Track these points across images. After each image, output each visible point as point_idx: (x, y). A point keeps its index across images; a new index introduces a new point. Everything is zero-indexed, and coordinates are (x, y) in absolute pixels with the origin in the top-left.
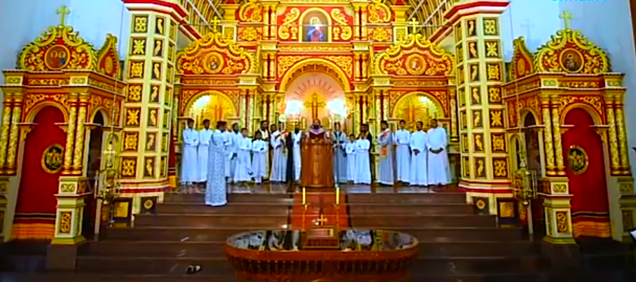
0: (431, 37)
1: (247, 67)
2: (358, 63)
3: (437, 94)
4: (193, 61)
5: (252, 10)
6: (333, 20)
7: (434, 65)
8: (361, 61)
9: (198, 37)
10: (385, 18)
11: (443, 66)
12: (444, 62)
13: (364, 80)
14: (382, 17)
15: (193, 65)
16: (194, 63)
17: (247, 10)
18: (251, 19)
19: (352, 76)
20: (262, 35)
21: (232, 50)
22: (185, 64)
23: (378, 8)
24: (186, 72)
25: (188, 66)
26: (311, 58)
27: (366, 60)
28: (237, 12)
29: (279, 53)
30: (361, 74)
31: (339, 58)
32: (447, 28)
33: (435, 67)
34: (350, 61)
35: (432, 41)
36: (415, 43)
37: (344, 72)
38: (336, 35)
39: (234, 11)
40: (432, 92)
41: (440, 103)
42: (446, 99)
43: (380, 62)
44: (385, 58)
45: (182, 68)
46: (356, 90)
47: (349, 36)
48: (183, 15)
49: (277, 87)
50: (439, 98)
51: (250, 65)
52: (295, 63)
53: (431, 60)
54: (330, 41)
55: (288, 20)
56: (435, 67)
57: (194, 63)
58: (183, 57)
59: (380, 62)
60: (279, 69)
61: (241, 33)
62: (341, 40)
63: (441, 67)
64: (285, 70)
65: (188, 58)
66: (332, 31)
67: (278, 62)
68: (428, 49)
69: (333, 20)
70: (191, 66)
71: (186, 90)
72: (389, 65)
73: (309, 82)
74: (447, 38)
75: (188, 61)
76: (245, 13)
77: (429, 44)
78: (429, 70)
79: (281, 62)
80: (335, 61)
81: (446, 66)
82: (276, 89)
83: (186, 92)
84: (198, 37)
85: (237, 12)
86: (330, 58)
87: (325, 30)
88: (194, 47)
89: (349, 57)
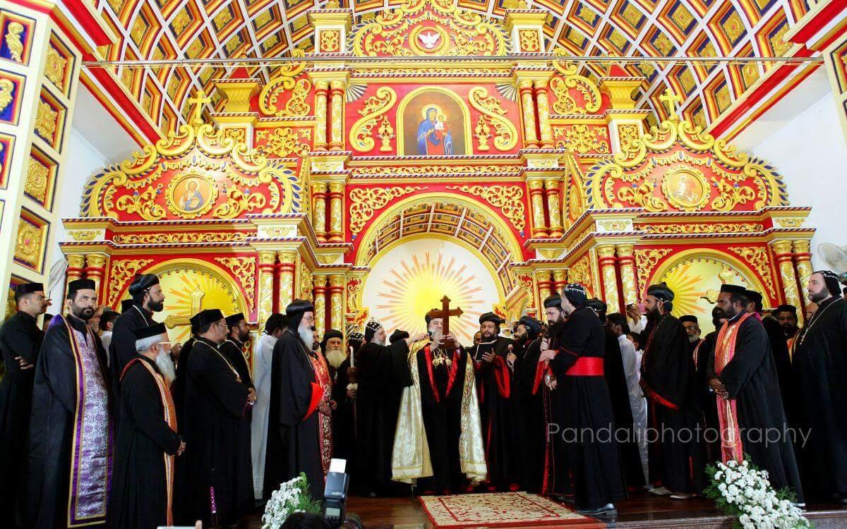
0: (711, 127)
1: (275, 200)
2: (537, 200)
3: (746, 252)
4: (141, 190)
5: (288, 93)
6: (472, 108)
7: (729, 188)
8: (544, 194)
9: (154, 138)
10: (589, 106)
11: (749, 190)
12: (749, 181)
13: (554, 235)
14: (582, 103)
15: (143, 200)
16: (145, 196)
17: (277, 92)
18: (287, 111)
19: (527, 229)
20: (311, 143)
21: (239, 163)
22: (123, 199)
23: (572, 84)
24: (123, 215)
25: (129, 202)
26: (426, 191)
27: (558, 191)
28: (254, 100)
29: (352, 182)
30: (547, 222)
31: (492, 189)
32: (793, 68)
33: (731, 192)
34: (518, 197)
35: (716, 133)
36: (678, 139)
37: (507, 220)
38: (483, 140)
39: (246, 95)
40: (736, 250)
41: (756, 272)
42: (769, 265)
43: (603, 183)
44: (613, 174)
45: (114, 209)
46: (540, 257)
47: (512, 144)
48: (101, 38)
49: (351, 257)
50: (751, 261)
51: (282, 196)
52: (391, 203)
53: (719, 177)
54: (469, 151)
55: (370, 111)
56: (731, 192)
57: (145, 196)
58: (117, 182)
59: (603, 183)
60: (354, 217)
61: (263, 142)
62: (494, 150)
63: (744, 192)
64: (366, 218)
65: (129, 185)
66: (474, 132)
67: (349, 202)
68: (709, 153)
69: (472, 108)
70: (137, 203)
71: (120, 258)
72: (624, 190)
73: (415, 259)
74: (754, 123)
75: (131, 192)
76: (273, 99)
77: (710, 142)
78: (718, 199)
79: (357, 202)
80: (485, 195)
81: (757, 191)
82: (346, 260)
83: (121, 264)
84: (154, 138)
85: (254, 100)
86: (472, 190)
87: (455, 125)
88: (147, 159)
89: (516, 187)
